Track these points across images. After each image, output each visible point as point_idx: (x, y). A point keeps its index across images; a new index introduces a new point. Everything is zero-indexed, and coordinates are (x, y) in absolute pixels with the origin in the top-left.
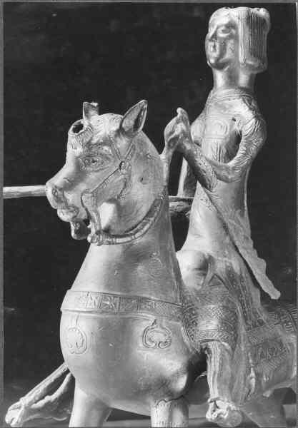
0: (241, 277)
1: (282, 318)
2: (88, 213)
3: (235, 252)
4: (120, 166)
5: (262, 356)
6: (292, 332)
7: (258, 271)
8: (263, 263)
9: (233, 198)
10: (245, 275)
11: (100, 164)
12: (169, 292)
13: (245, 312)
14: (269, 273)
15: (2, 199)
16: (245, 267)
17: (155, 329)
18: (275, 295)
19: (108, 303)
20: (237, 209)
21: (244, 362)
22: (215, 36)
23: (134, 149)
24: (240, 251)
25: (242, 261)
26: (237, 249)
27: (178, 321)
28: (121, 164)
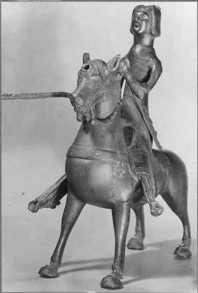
16: (149, 135)
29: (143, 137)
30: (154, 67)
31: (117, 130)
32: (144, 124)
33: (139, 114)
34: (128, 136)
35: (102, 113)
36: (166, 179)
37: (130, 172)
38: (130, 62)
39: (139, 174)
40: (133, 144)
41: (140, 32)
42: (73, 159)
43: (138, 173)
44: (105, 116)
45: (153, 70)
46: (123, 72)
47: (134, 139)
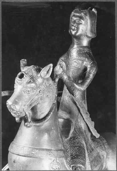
0: (85, 131)
1: (99, 144)
2: (26, 114)
3: (83, 120)
4: (39, 92)
5: (94, 165)
6: (103, 150)
7: (91, 127)
8: (93, 123)
9: (81, 95)
10: (87, 129)
11: (31, 90)
12: (59, 145)
13: (87, 147)
14: (96, 127)
15: (1, 97)
16: (86, 126)
17: (54, 163)
18: (97, 136)
19: (34, 153)
20: (83, 100)
21: (72, 70)
22: (31, 85)
23: (46, 84)
24: (85, 120)
25: (85, 124)
26: (84, 119)
27: (63, 158)
28: (40, 91)
29: (80, 129)
30: (89, 66)
31: (53, 128)
32: (81, 117)
33: (76, 108)
34: (67, 128)
35: (39, 114)
36: (69, 54)
37: (66, 164)
38: (65, 64)
39: (74, 166)
40: (70, 135)
41: (78, 34)
42: (13, 154)
43: (73, 165)
44: (42, 116)
45: (88, 69)
46: (59, 75)
47: (72, 131)
